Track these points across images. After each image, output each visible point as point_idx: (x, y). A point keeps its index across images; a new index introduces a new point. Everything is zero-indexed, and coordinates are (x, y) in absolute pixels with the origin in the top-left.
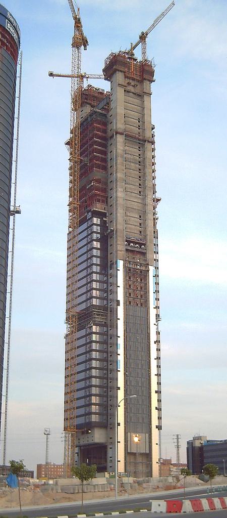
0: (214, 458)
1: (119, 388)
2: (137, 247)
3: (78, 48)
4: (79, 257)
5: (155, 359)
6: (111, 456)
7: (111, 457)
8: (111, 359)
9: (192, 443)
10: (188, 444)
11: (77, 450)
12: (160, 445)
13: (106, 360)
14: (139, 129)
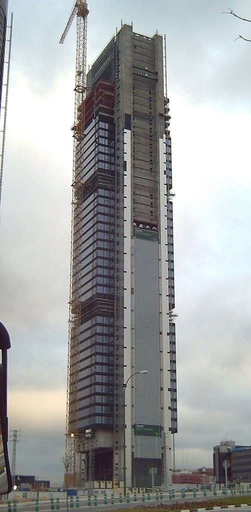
0: (243, 465)
2: (148, 229)
6: (116, 473)
7: (117, 464)
8: (118, 333)
9: (219, 448)
10: (214, 450)
14: (150, 108)
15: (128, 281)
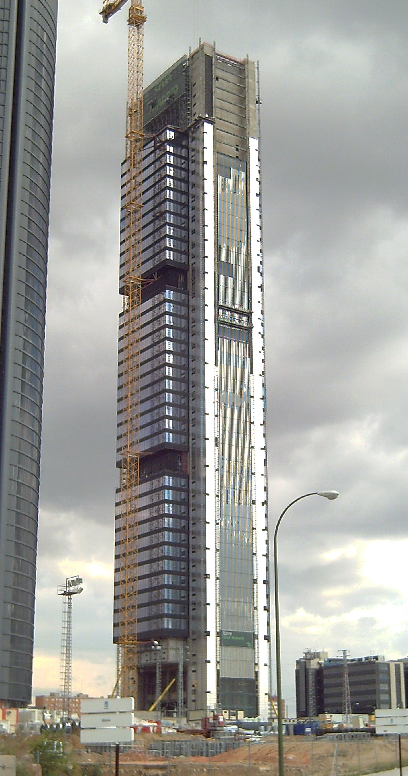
1: (208, 633)
3: (138, 26)
4: (144, 170)
5: (261, 425)
11: (133, 674)
12: (263, 304)
13: (185, 503)
15: (211, 428)
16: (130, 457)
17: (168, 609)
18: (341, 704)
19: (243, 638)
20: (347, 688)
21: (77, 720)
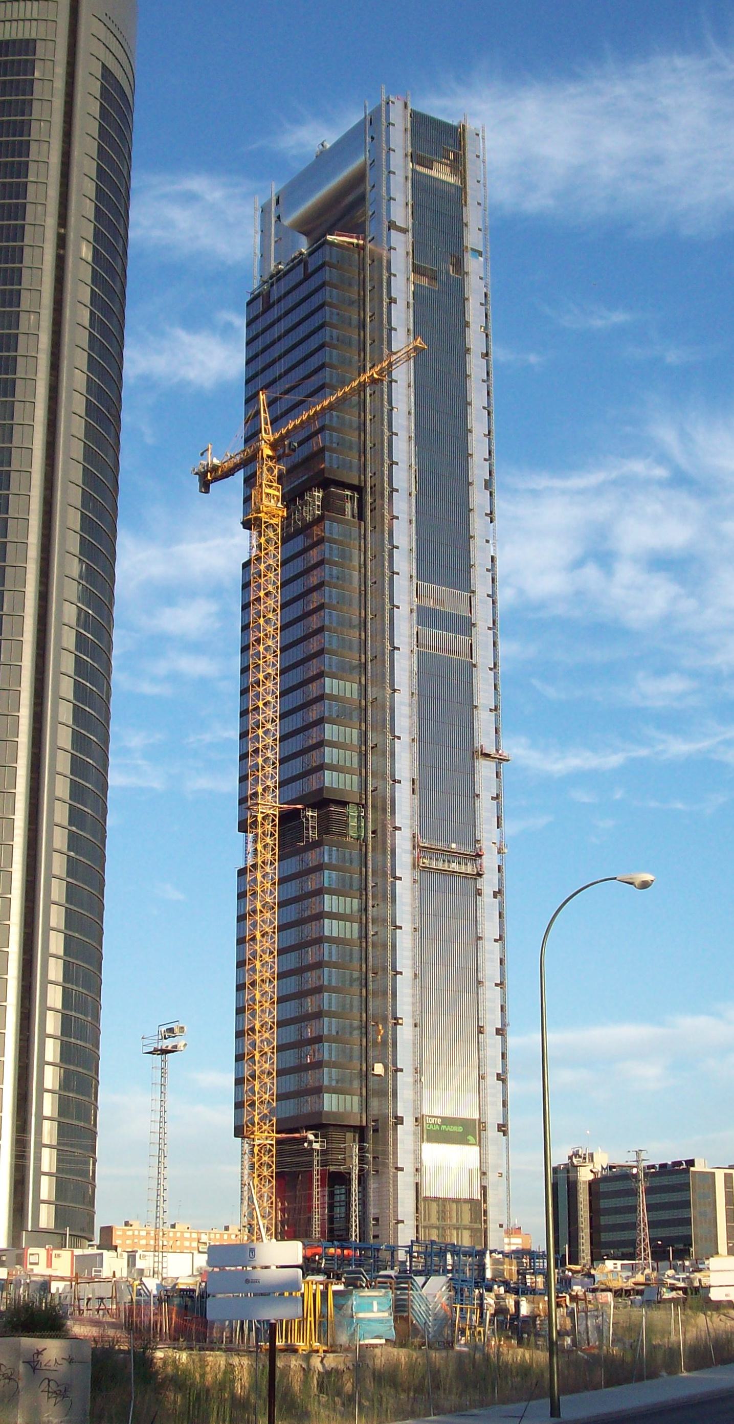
1: (399, 1120)
16: (262, 813)
17: (330, 1077)
18: (633, 1243)
19: (460, 1129)
20: (643, 1215)
21: (41, 1237)
